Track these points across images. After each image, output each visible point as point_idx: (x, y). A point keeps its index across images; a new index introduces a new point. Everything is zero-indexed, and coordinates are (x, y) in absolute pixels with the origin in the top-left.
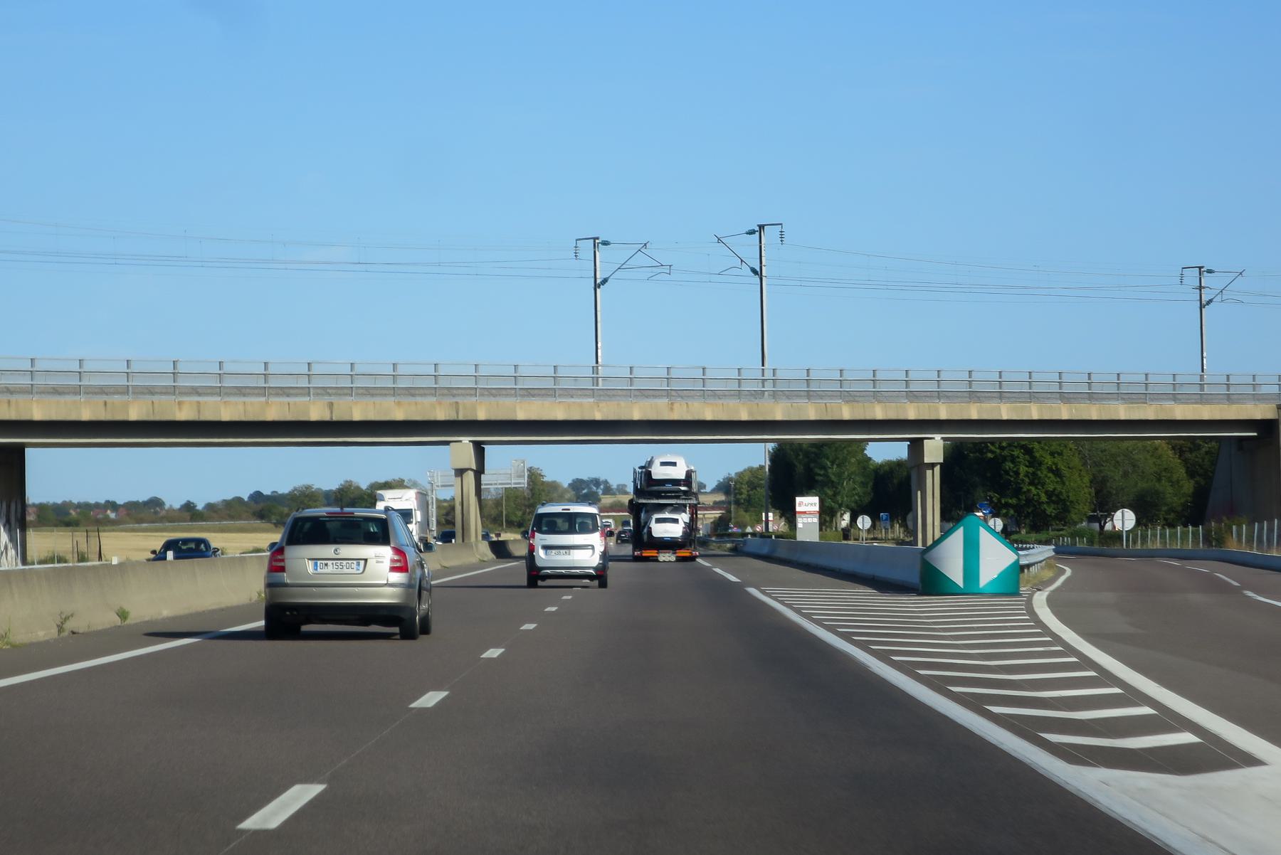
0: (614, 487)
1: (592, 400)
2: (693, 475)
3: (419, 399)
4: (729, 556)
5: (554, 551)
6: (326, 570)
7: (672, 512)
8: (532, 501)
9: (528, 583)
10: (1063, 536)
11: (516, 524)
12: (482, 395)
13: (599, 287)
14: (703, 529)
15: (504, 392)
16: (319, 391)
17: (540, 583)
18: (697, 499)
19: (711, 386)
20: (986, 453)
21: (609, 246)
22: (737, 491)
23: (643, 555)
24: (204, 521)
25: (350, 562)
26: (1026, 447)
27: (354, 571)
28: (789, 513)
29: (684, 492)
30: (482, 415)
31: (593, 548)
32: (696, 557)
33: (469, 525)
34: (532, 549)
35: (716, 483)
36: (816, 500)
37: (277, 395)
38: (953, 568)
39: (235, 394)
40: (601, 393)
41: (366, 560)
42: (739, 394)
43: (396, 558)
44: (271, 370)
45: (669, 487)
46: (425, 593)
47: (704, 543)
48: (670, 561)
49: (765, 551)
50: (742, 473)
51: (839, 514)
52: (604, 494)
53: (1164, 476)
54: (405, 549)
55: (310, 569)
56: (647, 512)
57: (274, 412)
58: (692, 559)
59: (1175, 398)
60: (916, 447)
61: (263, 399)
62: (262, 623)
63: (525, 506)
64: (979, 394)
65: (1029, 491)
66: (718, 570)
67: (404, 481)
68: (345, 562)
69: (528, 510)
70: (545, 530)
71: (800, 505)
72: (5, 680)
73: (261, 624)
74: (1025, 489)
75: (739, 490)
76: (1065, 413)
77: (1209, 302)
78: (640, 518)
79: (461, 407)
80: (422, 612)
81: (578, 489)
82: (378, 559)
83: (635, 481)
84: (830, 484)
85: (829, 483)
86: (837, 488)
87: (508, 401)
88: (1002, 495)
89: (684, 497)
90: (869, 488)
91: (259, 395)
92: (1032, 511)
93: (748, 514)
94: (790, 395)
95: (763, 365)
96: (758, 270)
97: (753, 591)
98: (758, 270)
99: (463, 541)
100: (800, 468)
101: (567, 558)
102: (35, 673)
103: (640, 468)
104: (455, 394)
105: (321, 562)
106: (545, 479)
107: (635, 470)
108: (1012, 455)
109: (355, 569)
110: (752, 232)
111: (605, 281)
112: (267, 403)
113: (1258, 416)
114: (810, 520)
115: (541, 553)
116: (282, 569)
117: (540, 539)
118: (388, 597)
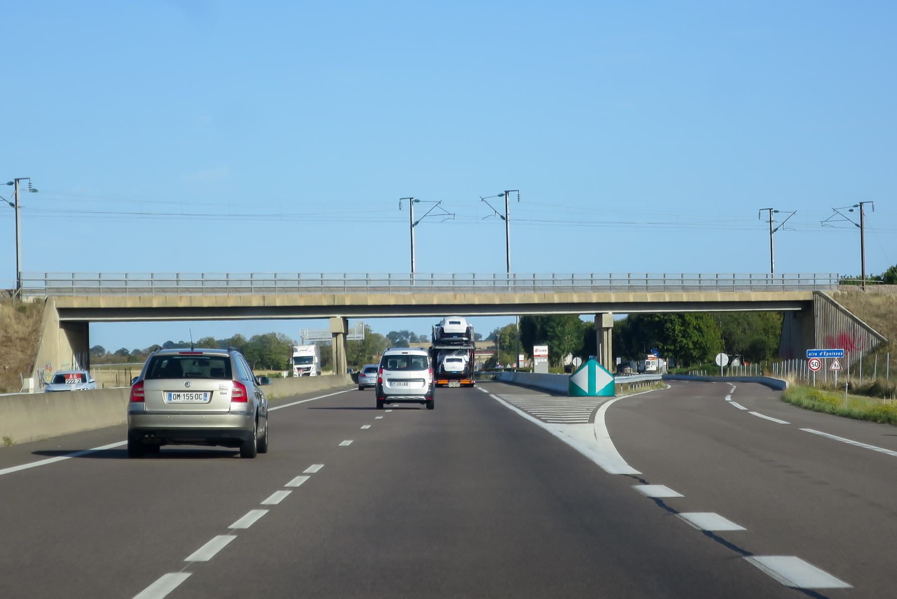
0: (419, 337)
1: (410, 293)
2: (471, 331)
3: (312, 293)
4: (489, 382)
5: (396, 383)
6: (177, 401)
7: (458, 354)
8: (363, 348)
10: (695, 370)
11: (352, 363)
12: (347, 291)
13: (413, 226)
14: (478, 365)
15: (360, 289)
16: (257, 289)
17: (385, 405)
18: (474, 346)
19: (477, 285)
20: (654, 318)
21: (419, 203)
22: (502, 340)
23: (439, 383)
24: (137, 362)
25: (199, 393)
26: (680, 316)
27: (202, 401)
28: (530, 355)
29: (466, 341)
30: (348, 302)
31: (424, 380)
32: (473, 384)
33: (341, 364)
34: (380, 381)
35: (489, 334)
36: (546, 348)
37: (233, 291)
38: (584, 384)
39: (210, 292)
40: (414, 288)
41: (212, 392)
42: (494, 289)
43: (237, 390)
44: (230, 278)
45: (455, 338)
46: (261, 419)
47: (478, 375)
48: (456, 387)
49: (510, 379)
50: (506, 328)
51: (562, 357)
52: (411, 342)
53: (771, 332)
54: (244, 383)
55: (166, 400)
56: (441, 354)
57: (232, 301)
58: (471, 385)
59: (751, 288)
60: (599, 317)
61: (226, 294)
62: (125, 442)
63: (359, 350)
64: (634, 287)
65: (682, 341)
66: (480, 388)
67: (276, 334)
68: (194, 394)
69: (360, 354)
71: (536, 351)
72: (12, 468)
73: (358, 388)
74: (679, 340)
75: (504, 339)
76: (685, 298)
78: (436, 359)
79: (336, 298)
80: (259, 435)
81: (393, 339)
82: (222, 391)
83: (433, 335)
84: (557, 338)
85: (555, 336)
86: (561, 340)
87: (363, 294)
88: (665, 343)
89: (465, 345)
90: (582, 340)
91: (223, 292)
92: (684, 354)
93: (510, 356)
94: (524, 289)
95: (508, 272)
96: (505, 217)
97: (493, 396)
98: (505, 217)
99: (337, 373)
100: (539, 327)
102: (44, 461)
103: (436, 325)
104: (333, 290)
105: (188, 393)
106: (372, 332)
107: (433, 329)
108: (670, 319)
109: (203, 399)
110: (501, 195)
111: (417, 223)
112: (228, 296)
113: (801, 299)
114: (542, 360)
115: (387, 384)
116: (142, 399)
117: (387, 374)
118: (230, 422)
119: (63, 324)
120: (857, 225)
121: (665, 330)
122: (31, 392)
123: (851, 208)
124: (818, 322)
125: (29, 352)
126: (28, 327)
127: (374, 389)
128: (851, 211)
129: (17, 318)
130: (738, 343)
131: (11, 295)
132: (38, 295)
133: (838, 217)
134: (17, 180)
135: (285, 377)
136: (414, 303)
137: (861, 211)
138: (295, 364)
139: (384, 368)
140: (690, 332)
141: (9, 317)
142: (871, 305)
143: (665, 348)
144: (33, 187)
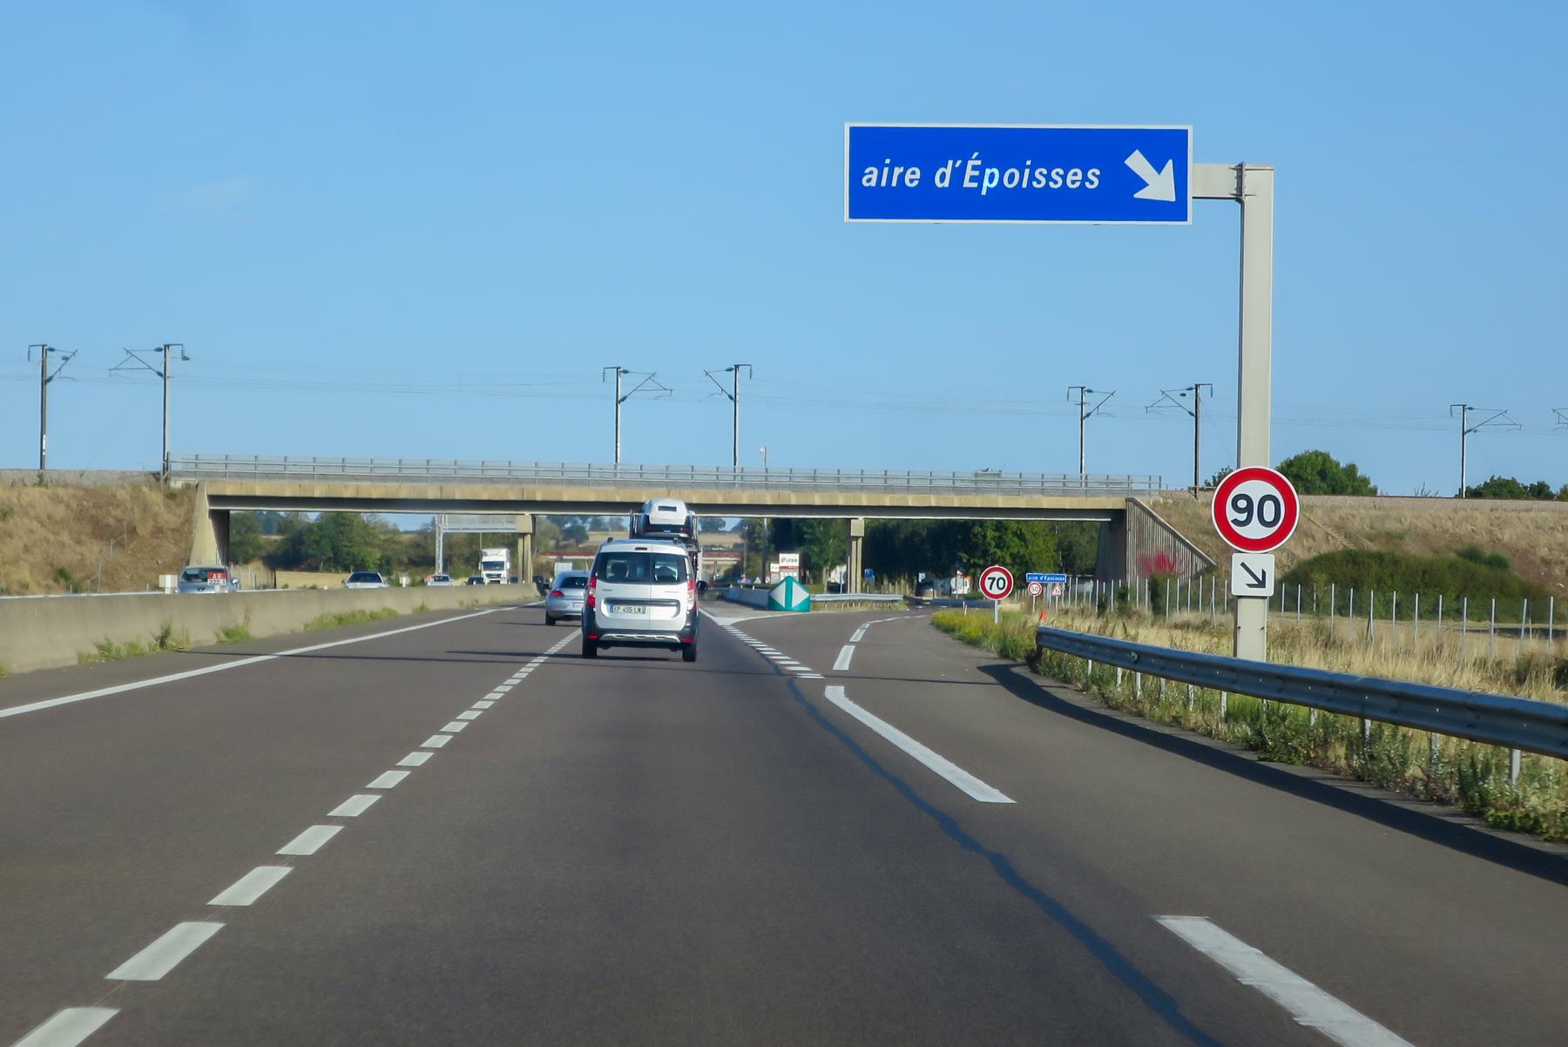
1: (613, 488)
3: (498, 486)
5: (622, 607)
9: (583, 652)
17: (600, 652)
30: (539, 498)
31: (678, 604)
34: (591, 602)
36: (796, 556)
42: (716, 485)
51: (825, 570)
59: (1043, 491)
61: (397, 484)
65: (995, 553)
70: (611, 577)
74: (991, 552)
77: (1088, 415)
87: (558, 488)
94: (753, 486)
95: (735, 464)
96: (733, 396)
98: (733, 396)
101: (641, 617)
110: (730, 370)
111: (623, 399)
112: (400, 486)
115: (604, 609)
117: (604, 589)
119: (213, 514)
120: (1191, 414)
121: (972, 536)
122: (168, 592)
123: (1182, 392)
124: (1131, 539)
125: (183, 545)
126: (179, 517)
127: (580, 623)
128: (1184, 395)
129: (168, 507)
130: (1081, 558)
131: (158, 480)
132: (188, 479)
133: (1169, 402)
134: (167, 346)
135: (404, 586)
136: (618, 499)
137: (1196, 396)
138: (485, 570)
139: (599, 578)
140: (1007, 540)
141: (157, 504)
142: (1200, 518)
143: (972, 562)
144: (186, 355)
